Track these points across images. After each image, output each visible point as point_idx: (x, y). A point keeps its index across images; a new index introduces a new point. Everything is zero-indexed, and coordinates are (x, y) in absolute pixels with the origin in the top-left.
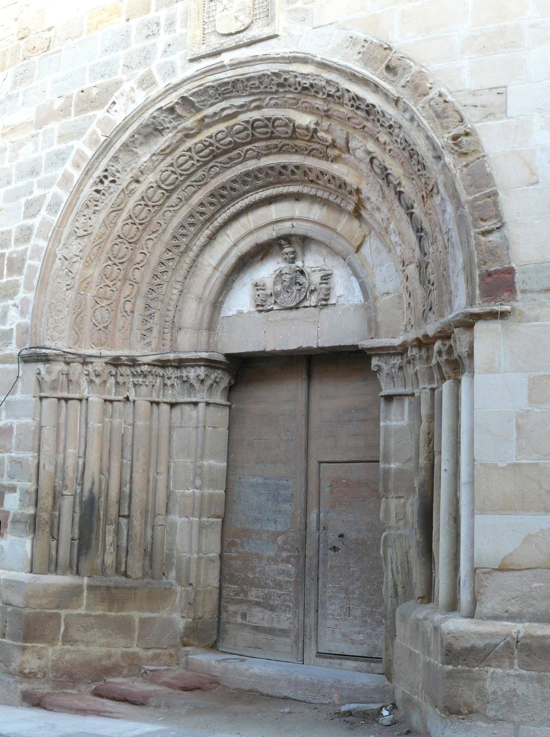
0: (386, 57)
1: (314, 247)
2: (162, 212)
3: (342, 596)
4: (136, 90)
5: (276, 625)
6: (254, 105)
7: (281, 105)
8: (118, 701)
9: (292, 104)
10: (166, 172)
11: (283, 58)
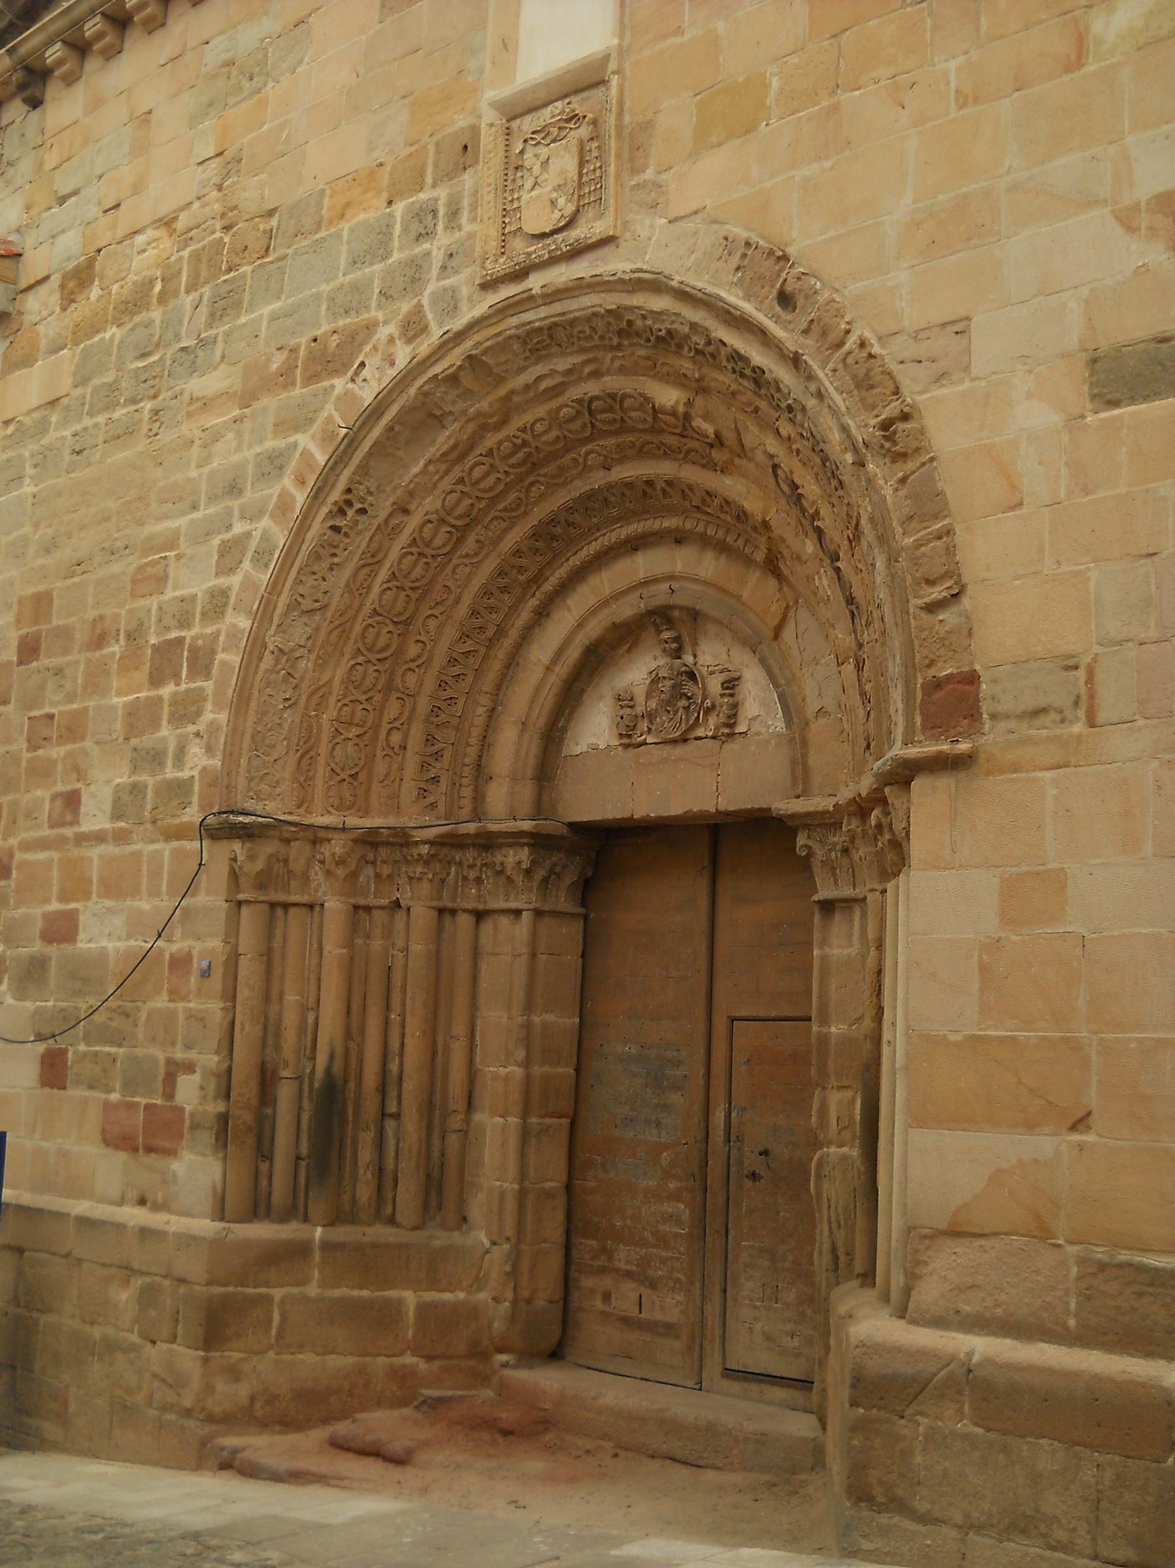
1: (712, 628)
3: (766, 1263)
6: (587, 370)
11: (621, 281)
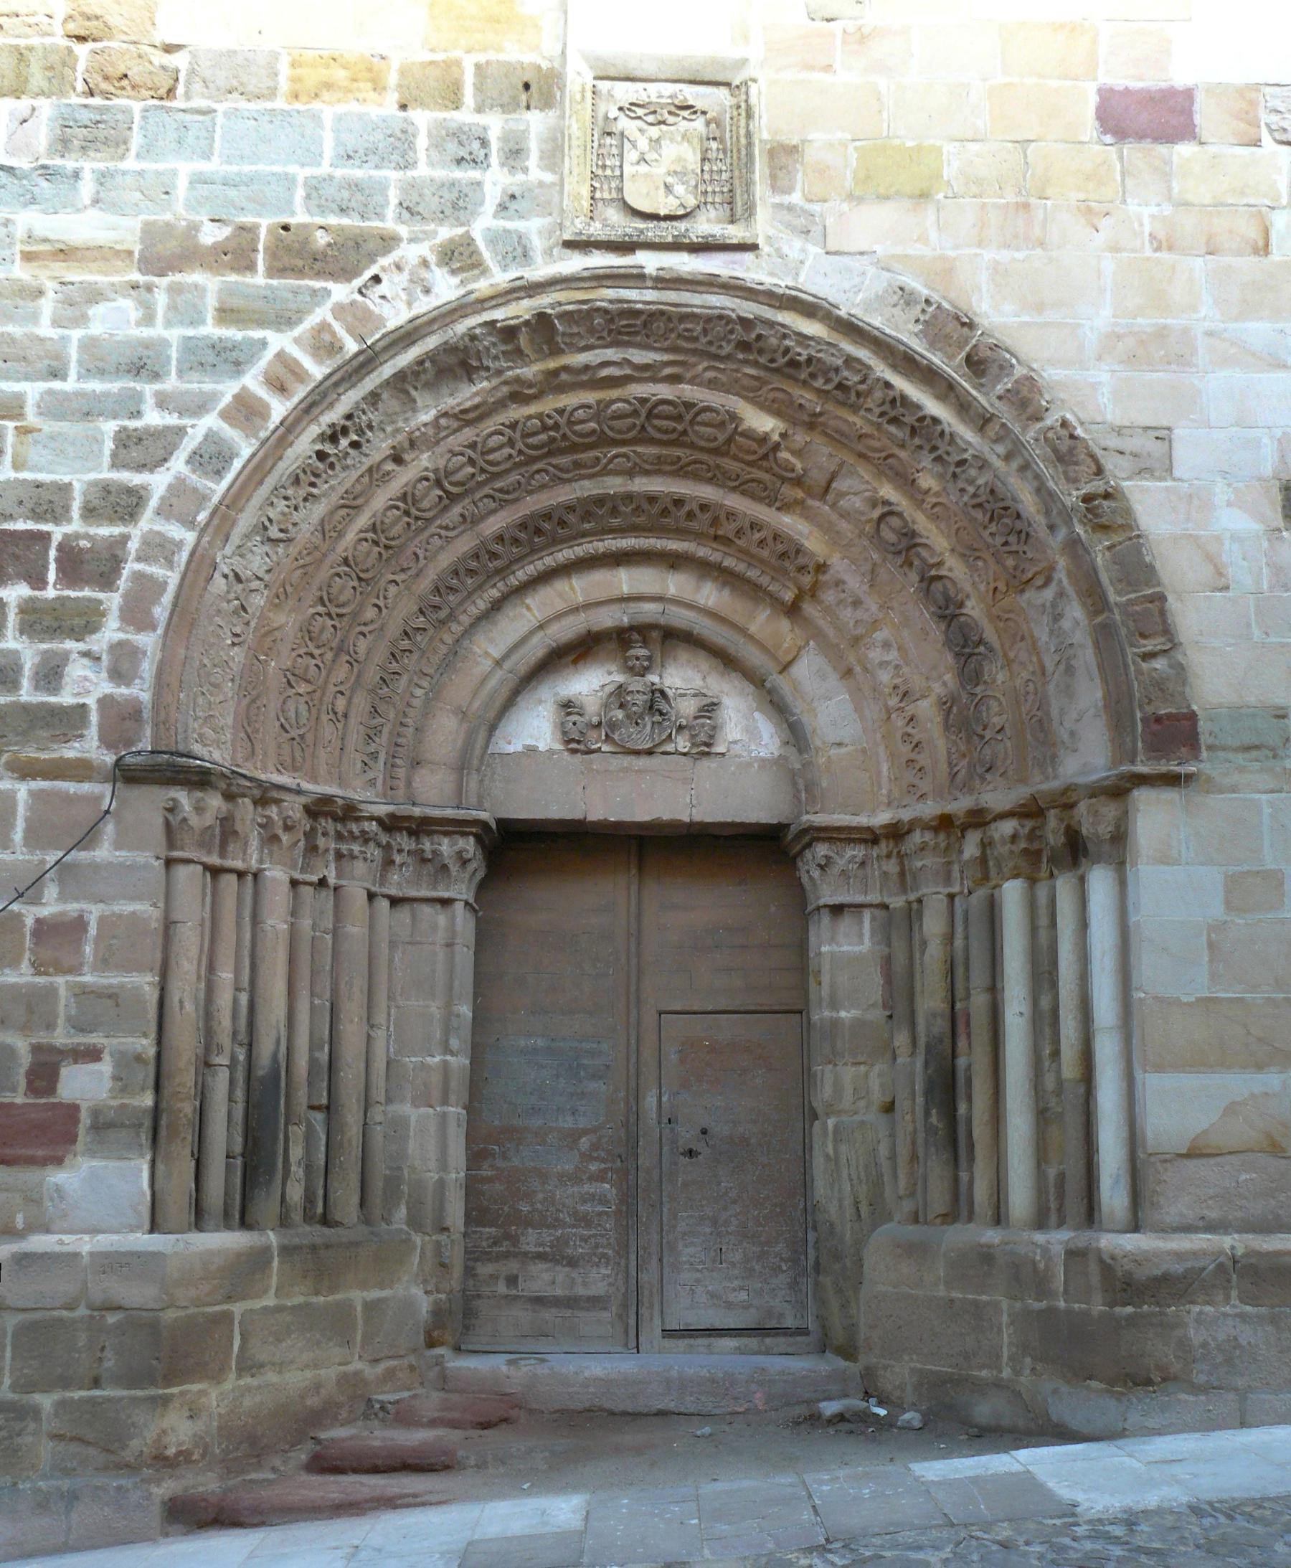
0: (967, 342)
2: (426, 534)
3: (708, 1230)
4: (433, 267)
5: (580, 1291)
6: (668, 371)
7: (723, 385)
8: (384, 1472)
9: (745, 388)
10: (460, 458)
